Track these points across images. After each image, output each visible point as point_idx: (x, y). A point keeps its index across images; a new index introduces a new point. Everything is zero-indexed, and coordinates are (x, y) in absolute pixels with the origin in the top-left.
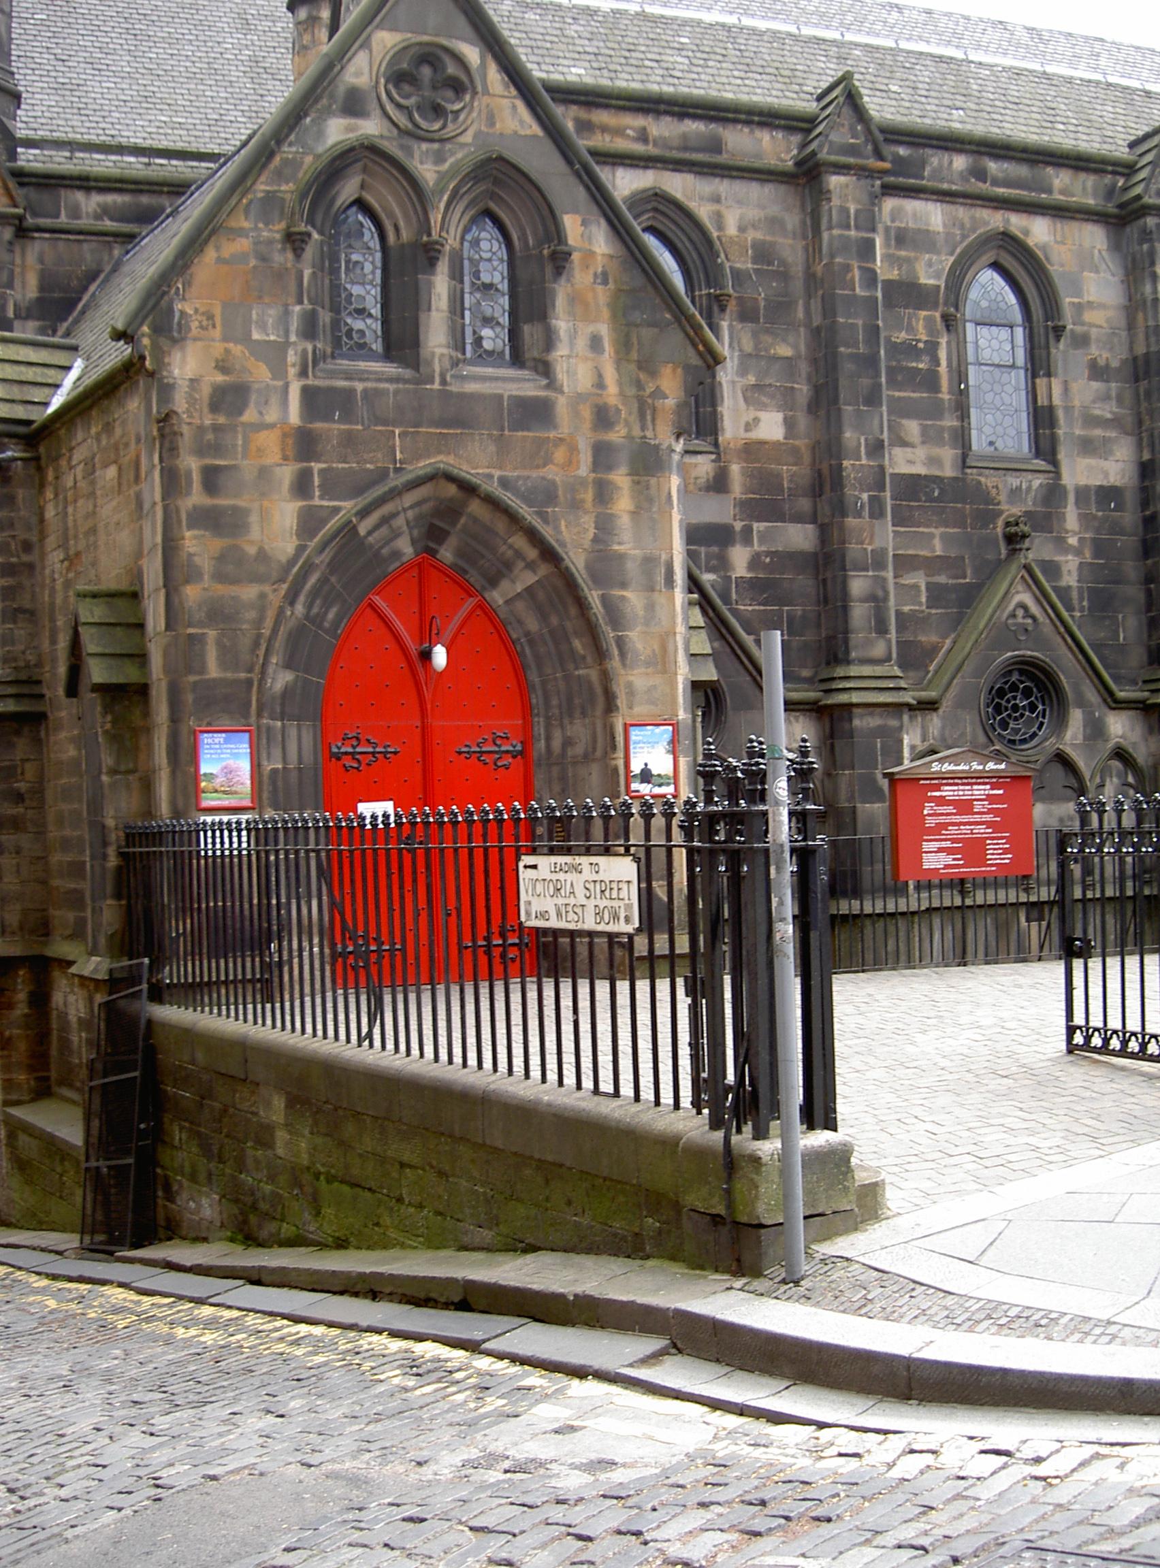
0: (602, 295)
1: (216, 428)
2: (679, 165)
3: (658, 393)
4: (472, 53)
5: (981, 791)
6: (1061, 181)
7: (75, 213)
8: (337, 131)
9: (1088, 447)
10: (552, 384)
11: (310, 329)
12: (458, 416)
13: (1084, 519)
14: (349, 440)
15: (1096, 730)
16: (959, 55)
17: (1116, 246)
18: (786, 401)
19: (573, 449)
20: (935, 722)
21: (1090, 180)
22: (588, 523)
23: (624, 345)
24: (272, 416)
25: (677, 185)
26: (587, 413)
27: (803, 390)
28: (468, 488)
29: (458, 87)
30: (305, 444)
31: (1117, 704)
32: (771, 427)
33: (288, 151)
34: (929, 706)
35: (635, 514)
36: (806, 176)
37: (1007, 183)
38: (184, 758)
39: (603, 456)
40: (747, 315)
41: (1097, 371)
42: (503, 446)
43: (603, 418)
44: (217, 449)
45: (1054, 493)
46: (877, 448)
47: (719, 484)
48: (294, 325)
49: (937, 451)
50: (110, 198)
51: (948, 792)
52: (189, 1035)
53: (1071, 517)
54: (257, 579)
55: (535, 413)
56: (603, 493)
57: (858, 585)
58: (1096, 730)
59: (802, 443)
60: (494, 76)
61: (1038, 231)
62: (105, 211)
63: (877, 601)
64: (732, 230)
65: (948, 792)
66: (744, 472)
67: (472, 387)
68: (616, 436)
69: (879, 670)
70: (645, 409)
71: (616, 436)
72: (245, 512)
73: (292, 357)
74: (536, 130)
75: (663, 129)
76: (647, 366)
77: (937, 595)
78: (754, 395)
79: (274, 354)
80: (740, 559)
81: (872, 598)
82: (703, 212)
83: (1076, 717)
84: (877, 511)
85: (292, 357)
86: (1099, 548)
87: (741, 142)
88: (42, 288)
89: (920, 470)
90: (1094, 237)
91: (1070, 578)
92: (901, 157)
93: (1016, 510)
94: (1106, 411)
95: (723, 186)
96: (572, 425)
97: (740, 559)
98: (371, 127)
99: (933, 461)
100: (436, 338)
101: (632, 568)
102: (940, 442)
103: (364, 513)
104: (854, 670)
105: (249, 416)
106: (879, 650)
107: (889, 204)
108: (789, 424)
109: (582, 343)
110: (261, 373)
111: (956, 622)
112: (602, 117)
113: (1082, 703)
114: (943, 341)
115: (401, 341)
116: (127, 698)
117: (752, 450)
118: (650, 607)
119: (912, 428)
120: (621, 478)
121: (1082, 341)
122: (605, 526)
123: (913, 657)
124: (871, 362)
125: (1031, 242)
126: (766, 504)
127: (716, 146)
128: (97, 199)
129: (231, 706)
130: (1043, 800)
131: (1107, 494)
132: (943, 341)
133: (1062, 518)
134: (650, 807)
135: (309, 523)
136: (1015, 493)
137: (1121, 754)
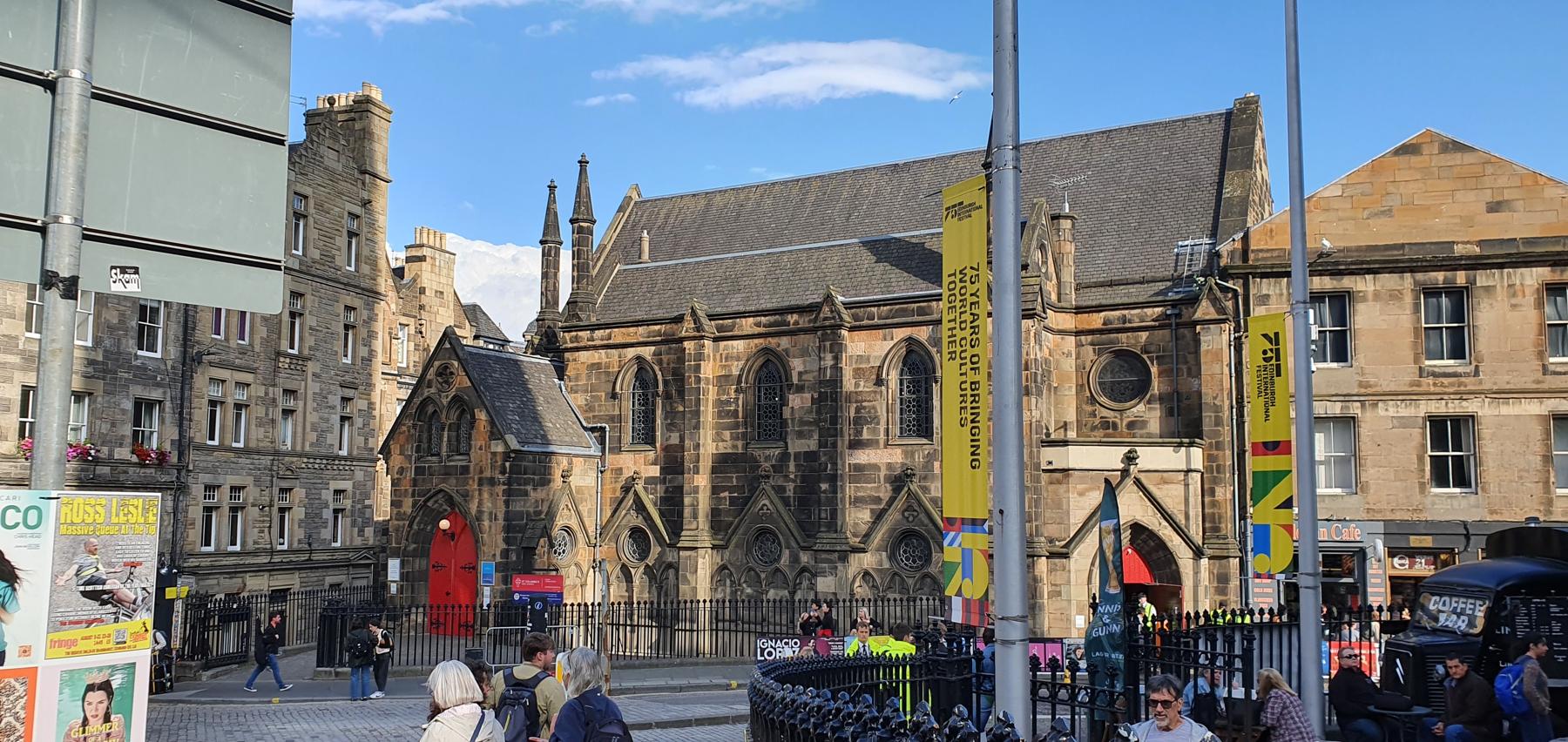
6: (792, 318)
9: (800, 435)
15: (795, 559)
30: (415, 482)
31: (804, 549)
53: (792, 468)
55: (465, 470)
57: (687, 500)
83: (786, 553)
99: (735, 447)
131: (810, 456)
136: (767, 458)
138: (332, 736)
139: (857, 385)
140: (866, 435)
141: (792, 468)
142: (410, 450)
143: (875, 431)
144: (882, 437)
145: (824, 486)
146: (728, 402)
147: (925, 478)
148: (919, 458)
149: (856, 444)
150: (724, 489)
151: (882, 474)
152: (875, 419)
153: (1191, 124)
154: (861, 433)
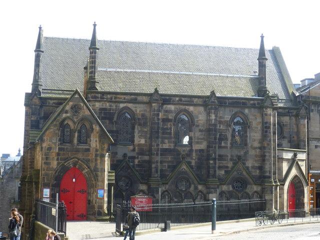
0: (98, 135)
1: (48, 152)
2: (130, 103)
3: (104, 147)
4: (82, 104)
5: (144, 200)
6: (195, 100)
7: (49, 103)
8: (64, 115)
9: (198, 143)
10: (90, 146)
11: (60, 140)
12: (78, 151)
13: (196, 155)
14: (64, 154)
16: (191, 73)
17: (205, 110)
18: (145, 138)
19: (92, 154)
20: (167, 186)
21: (201, 100)
22: (94, 164)
23: (100, 141)
24: (54, 151)
25: (130, 105)
26: (94, 150)
27: (148, 135)
28: (79, 159)
29: (80, 109)
30: (58, 154)
32: (143, 141)
33: (58, 118)
34: (167, 184)
35: (100, 163)
36: (149, 103)
37: (186, 102)
38: (42, 192)
39: (96, 155)
40: (140, 125)
41: (200, 131)
42: (83, 154)
43: (97, 150)
44: (48, 155)
45: (191, 151)
46: (158, 145)
47: (134, 150)
48: (58, 139)
49: (171, 144)
50: (54, 101)
51: (139, 200)
52: (39, 225)
53: (194, 154)
54: (51, 170)
55: (88, 150)
56: (96, 160)
57: (153, 166)
58: (196, 188)
59: (148, 144)
60: (85, 107)
61: (191, 108)
62: (54, 103)
63: (156, 168)
64: (138, 112)
65: (139, 200)
66: (138, 148)
67: (80, 147)
68: (98, 153)
69: (156, 179)
70: (102, 149)
71: (98, 153)
72: (50, 163)
73: (57, 144)
74: (90, 114)
75: (127, 97)
76: (103, 144)
77: (169, 167)
78: (140, 137)
79: (55, 144)
80: (136, 161)
81: (155, 168)
82: (134, 109)
83: (193, 186)
84: (157, 154)
85: (57, 144)
86: (199, 159)
87: (140, 98)
88: (44, 115)
89: (167, 147)
90: (202, 109)
91: (193, 163)
92: (167, 99)
93: (184, 153)
94: (202, 137)
95: (137, 105)
96: (93, 152)
97: (136, 161)
98: (68, 115)
99: (169, 146)
100: (75, 141)
101: (100, 170)
102: (171, 143)
103: (65, 163)
104: (152, 179)
105: (52, 151)
106: (156, 175)
107: (165, 106)
108: (146, 141)
109: (94, 142)
110: (53, 146)
111: (172, 171)
112: (118, 96)
113: (194, 183)
114: (173, 127)
115: (71, 142)
116: (37, 183)
117: (139, 145)
118: (102, 174)
119: (166, 141)
120: (98, 158)
121: (198, 126)
122: (96, 164)
123: (163, 176)
124: (158, 132)
125: (190, 111)
126: (142, 153)
127: (136, 99)
128: (52, 101)
129: (46, 186)
130: (186, 199)
131: (201, 151)
132: (173, 127)
133: (192, 154)
134: (26, 214)
135: (58, 164)
136: (184, 151)
137: (200, 191)
138: (56, 237)
139: (220, 127)
140: (223, 144)
141: (194, 154)
142: (56, 140)
143: (226, 143)
144: (229, 145)
145: (211, 162)
146: (167, 129)
147: (244, 160)
148: (242, 153)
149: (220, 147)
150: (165, 162)
151: (229, 158)
152: (227, 139)
153: (48, 39)
154: (221, 143)
